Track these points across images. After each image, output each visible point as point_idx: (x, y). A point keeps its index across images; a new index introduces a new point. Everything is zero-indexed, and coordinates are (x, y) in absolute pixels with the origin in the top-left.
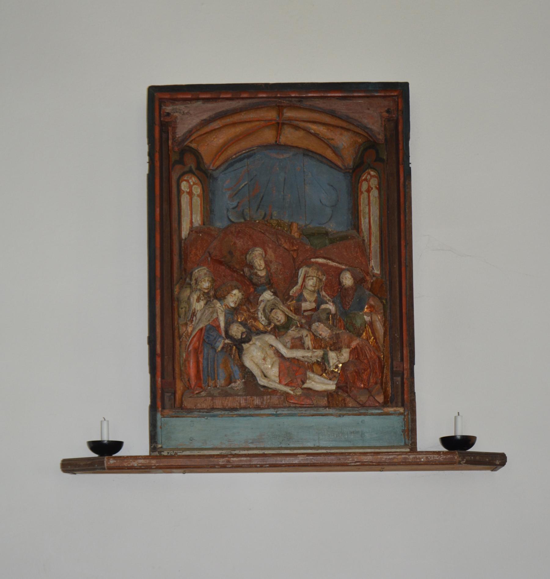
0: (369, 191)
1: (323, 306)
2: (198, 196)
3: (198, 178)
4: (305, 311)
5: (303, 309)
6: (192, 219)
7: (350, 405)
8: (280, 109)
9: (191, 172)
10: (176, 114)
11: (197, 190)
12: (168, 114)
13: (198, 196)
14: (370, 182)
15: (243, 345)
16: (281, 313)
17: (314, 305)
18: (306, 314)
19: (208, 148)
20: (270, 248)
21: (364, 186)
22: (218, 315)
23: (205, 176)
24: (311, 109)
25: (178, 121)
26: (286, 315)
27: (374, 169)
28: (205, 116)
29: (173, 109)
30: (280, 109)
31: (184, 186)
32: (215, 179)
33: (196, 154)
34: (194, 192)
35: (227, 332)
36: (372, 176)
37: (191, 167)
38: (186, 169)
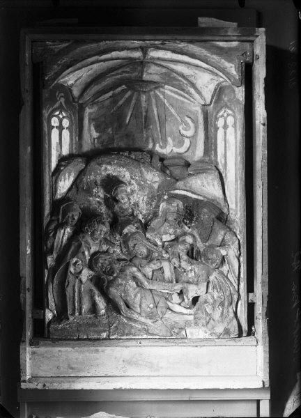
0: (225, 127)
9: (61, 108)
17: (173, 237)
21: (220, 123)
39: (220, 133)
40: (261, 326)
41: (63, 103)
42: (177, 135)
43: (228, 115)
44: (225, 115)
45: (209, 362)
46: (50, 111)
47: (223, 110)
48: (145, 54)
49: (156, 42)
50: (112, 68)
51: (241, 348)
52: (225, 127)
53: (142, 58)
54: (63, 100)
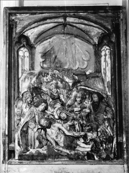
0: (105, 55)
1: (84, 110)
2: (28, 57)
3: (27, 48)
4: (76, 112)
5: (75, 111)
6: (21, 76)
7: (81, 81)
8: (65, 17)
9: (24, 46)
10: (16, 20)
11: (27, 54)
12: (13, 20)
13: (28, 57)
14: (106, 51)
15: (47, 129)
16: (65, 114)
17: (80, 109)
18: (76, 113)
19: (32, 34)
20: (59, 81)
21: (103, 53)
22: (35, 115)
23: (31, 47)
24: (80, 17)
25: (17, 23)
26: (67, 115)
27: (108, 46)
28: (30, 21)
29: (15, 18)
30: (65, 17)
31: (21, 53)
32: (35, 48)
33: (27, 38)
34: (25, 55)
35: (39, 122)
36: (107, 49)
37: (24, 44)
38: (22, 45)
39: (103, 59)
40: (123, 94)
41: (25, 45)
42: (81, 59)
43: (107, 49)
44: (105, 49)
45: (105, 94)
46: (18, 48)
47: (104, 47)
48: (65, 20)
49: (71, 14)
50: (39, 34)
51: (115, 165)
52: (105, 55)
53: (64, 22)
54: (25, 43)
